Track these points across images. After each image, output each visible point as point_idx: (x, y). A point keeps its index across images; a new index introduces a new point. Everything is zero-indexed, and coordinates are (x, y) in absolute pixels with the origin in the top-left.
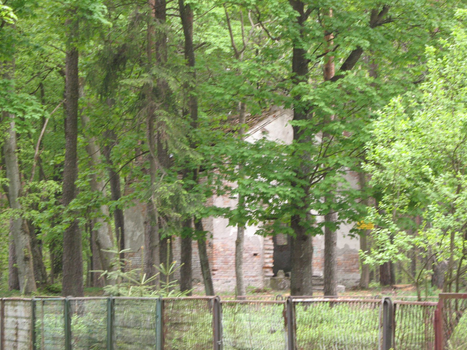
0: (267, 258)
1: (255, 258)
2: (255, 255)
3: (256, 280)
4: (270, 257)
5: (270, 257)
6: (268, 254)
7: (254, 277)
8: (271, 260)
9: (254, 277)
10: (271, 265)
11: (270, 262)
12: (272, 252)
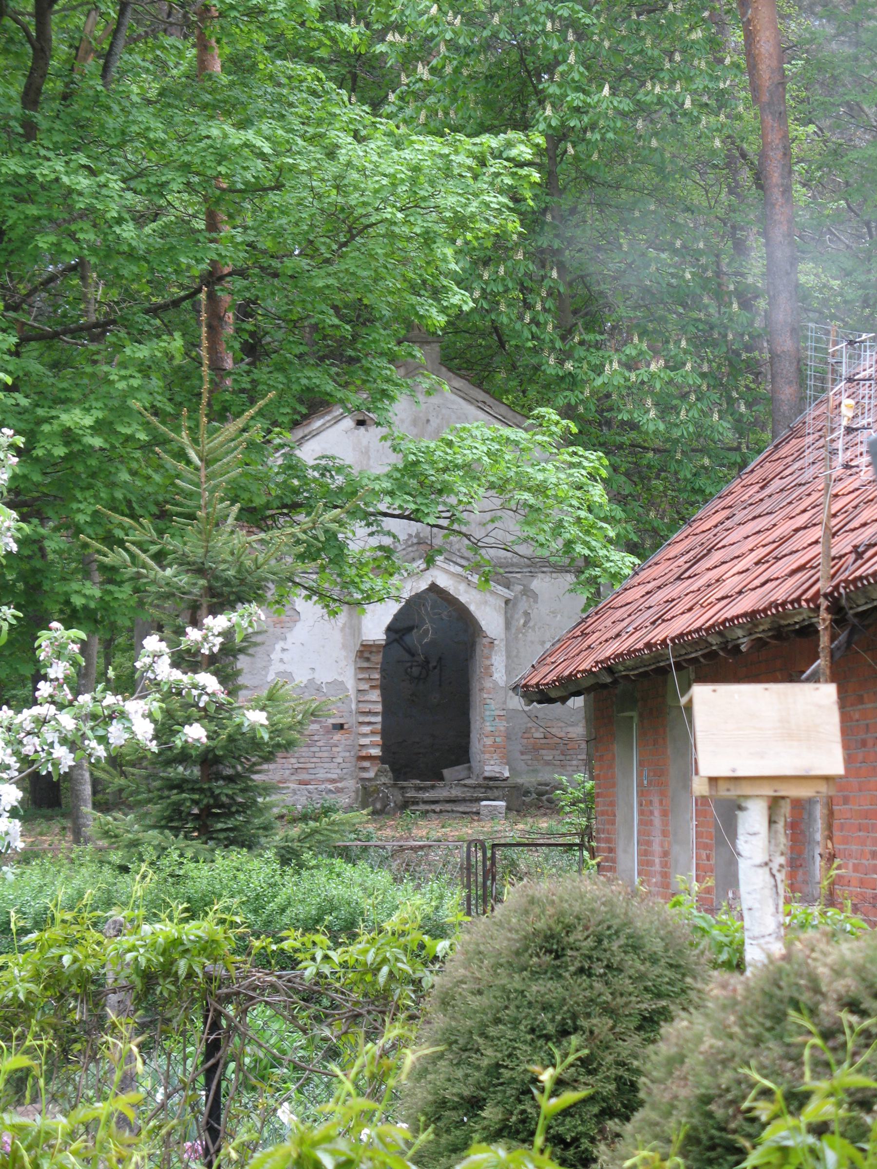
0: (365, 735)
1: (338, 736)
2: (341, 727)
3: (339, 791)
4: (373, 733)
5: (373, 733)
6: (369, 723)
7: (333, 781)
8: (377, 739)
9: (333, 781)
10: (376, 752)
11: (373, 745)
12: (379, 719)
